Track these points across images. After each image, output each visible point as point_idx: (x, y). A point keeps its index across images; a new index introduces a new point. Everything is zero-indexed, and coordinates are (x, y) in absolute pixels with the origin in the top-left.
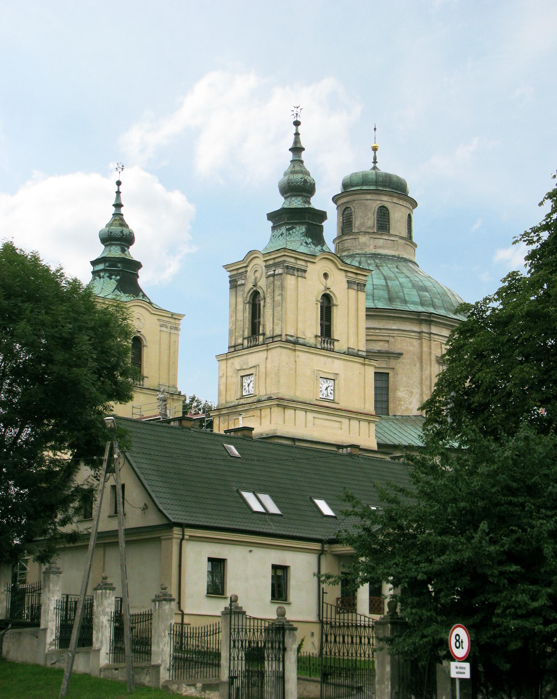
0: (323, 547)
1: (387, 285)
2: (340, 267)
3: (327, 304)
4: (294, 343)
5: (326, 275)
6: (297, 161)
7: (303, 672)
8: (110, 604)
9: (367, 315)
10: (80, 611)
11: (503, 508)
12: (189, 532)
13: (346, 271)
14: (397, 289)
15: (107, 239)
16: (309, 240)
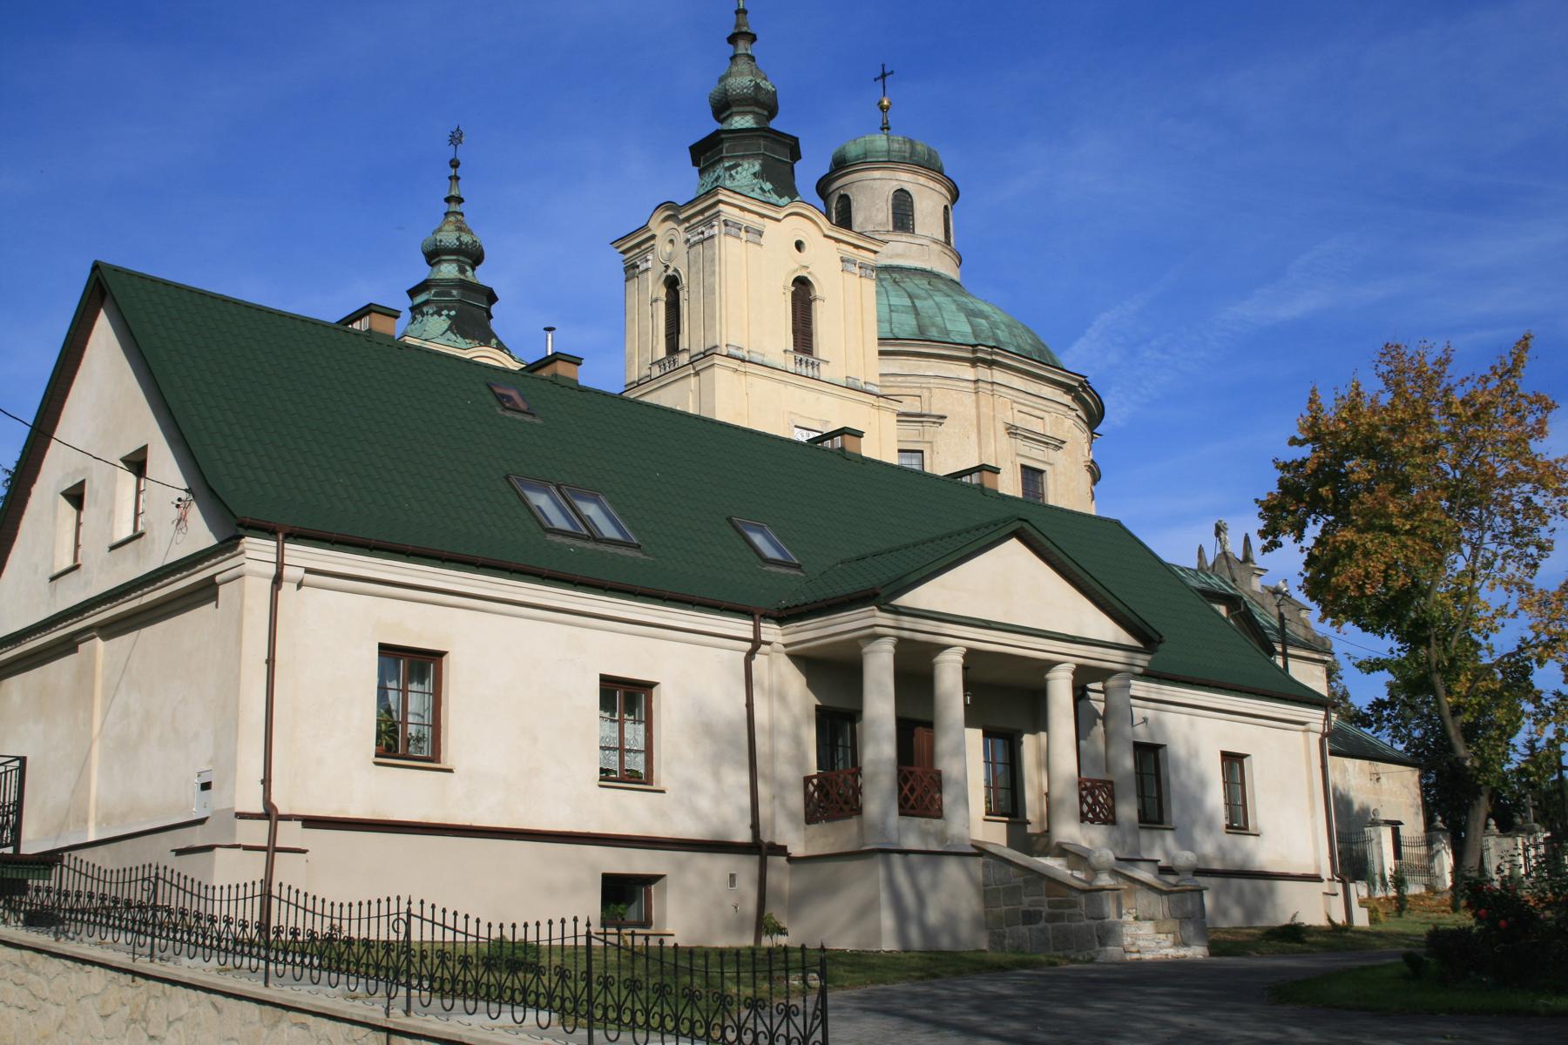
0: (757, 631)
1: (914, 306)
2: (828, 233)
3: (802, 291)
5: (799, 245)
7: (436, 1002)
9: (881, 353)
10: (989, 988)
13: (838, 240)
14: (931, 312)
16: (768, 186)
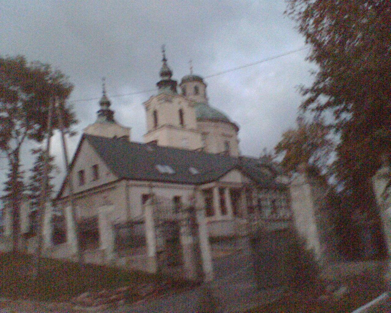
3: (181, 113)
4: (170, 127)
6: (165, 65)
8: (23, 129)
11: (355, 42)
12: (131, 182)
15: (102, 104)
